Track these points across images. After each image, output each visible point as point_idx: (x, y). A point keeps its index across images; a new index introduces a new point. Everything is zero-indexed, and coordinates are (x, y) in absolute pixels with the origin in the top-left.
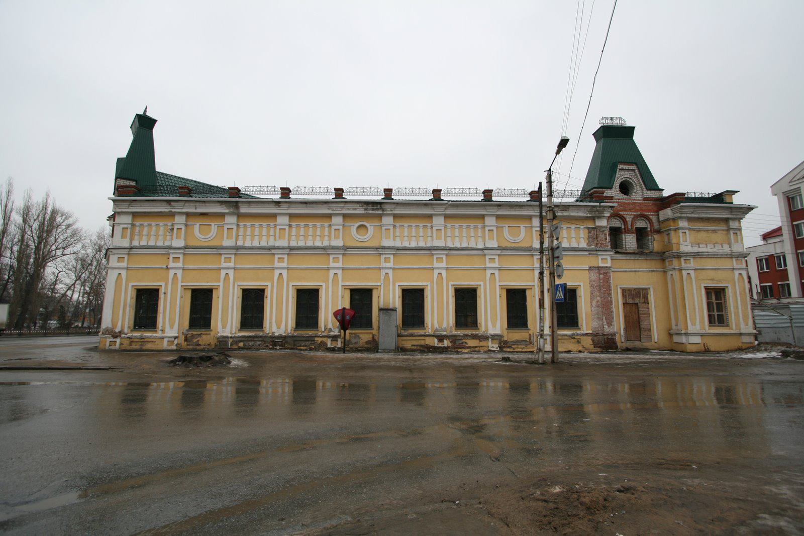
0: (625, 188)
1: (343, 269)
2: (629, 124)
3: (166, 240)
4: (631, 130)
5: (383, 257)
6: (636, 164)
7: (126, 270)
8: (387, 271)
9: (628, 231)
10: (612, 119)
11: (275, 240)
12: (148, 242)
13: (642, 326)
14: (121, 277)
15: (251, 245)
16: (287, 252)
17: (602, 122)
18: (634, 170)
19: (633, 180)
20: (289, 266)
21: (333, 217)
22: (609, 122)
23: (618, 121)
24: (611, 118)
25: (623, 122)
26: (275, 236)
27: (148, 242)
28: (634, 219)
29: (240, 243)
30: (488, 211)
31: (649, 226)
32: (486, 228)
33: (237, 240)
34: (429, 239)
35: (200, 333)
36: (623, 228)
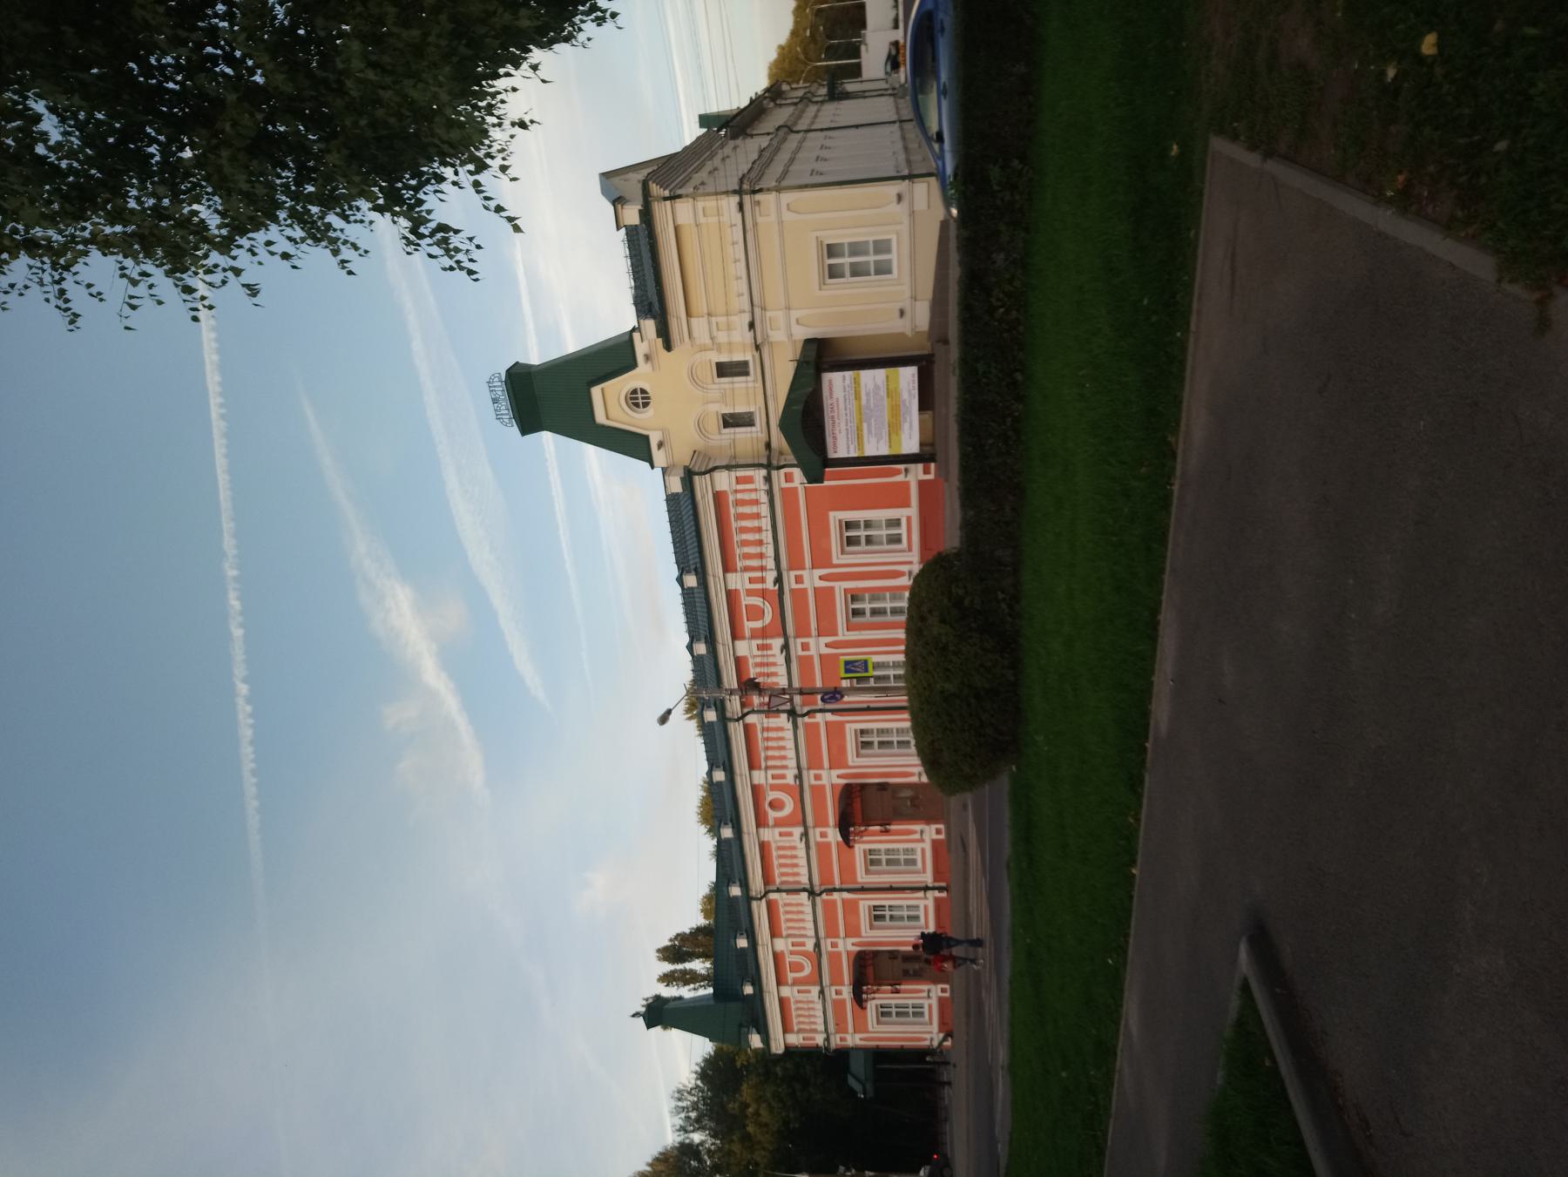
10: (495, 401)
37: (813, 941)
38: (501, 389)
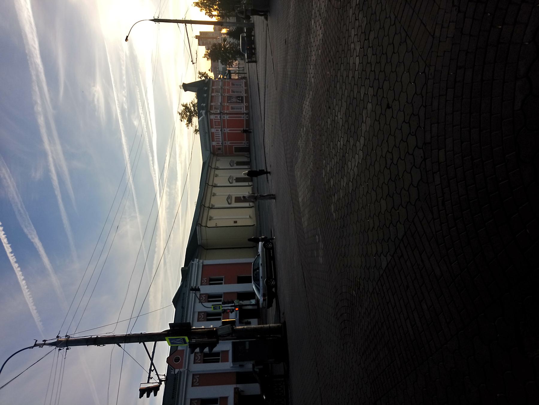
37: (221, 142)
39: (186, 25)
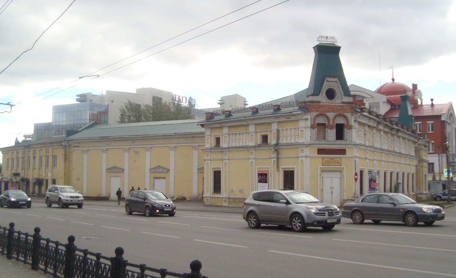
0: (331, 94)
1: (229, 160)
2: (338, 44)
3: (240, 142)
4: (338, 49)
5: (224, 153)
6: (338, 77)
7: (210, 161)
8: (251, 160)
9: (331, 127)
10: (327, 37)
11: (299, 138)
12: (246, 143)
13: (446, 157)
14: (226, 164)
15: (294, 142)
16: (254, 149)
17: (319, 39)
18: (336, 82)
19: (336, 88)
20: (255, 157)
21: (249, 126)
22: (324, 40)
23: (321, 39)
24: (326, 37)
25: (335, 41)
26: (298, 135)
27: (246, 143)
28: (335, 117)
29: (230, 145)
30: (298, 117)
31: (327, 123)
32: (299, 129)
33: (229, 143)
34: (297, 137)
35: (411, 158)
36: (346, 124)
38: (331, 41)
39: (393, 80)
